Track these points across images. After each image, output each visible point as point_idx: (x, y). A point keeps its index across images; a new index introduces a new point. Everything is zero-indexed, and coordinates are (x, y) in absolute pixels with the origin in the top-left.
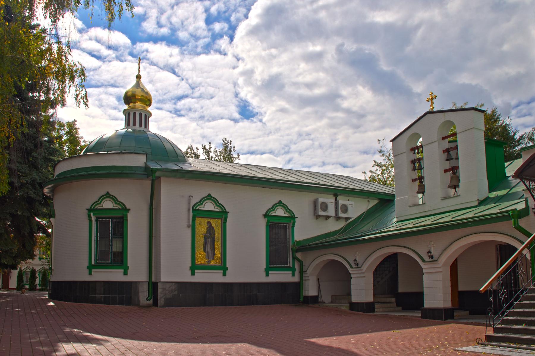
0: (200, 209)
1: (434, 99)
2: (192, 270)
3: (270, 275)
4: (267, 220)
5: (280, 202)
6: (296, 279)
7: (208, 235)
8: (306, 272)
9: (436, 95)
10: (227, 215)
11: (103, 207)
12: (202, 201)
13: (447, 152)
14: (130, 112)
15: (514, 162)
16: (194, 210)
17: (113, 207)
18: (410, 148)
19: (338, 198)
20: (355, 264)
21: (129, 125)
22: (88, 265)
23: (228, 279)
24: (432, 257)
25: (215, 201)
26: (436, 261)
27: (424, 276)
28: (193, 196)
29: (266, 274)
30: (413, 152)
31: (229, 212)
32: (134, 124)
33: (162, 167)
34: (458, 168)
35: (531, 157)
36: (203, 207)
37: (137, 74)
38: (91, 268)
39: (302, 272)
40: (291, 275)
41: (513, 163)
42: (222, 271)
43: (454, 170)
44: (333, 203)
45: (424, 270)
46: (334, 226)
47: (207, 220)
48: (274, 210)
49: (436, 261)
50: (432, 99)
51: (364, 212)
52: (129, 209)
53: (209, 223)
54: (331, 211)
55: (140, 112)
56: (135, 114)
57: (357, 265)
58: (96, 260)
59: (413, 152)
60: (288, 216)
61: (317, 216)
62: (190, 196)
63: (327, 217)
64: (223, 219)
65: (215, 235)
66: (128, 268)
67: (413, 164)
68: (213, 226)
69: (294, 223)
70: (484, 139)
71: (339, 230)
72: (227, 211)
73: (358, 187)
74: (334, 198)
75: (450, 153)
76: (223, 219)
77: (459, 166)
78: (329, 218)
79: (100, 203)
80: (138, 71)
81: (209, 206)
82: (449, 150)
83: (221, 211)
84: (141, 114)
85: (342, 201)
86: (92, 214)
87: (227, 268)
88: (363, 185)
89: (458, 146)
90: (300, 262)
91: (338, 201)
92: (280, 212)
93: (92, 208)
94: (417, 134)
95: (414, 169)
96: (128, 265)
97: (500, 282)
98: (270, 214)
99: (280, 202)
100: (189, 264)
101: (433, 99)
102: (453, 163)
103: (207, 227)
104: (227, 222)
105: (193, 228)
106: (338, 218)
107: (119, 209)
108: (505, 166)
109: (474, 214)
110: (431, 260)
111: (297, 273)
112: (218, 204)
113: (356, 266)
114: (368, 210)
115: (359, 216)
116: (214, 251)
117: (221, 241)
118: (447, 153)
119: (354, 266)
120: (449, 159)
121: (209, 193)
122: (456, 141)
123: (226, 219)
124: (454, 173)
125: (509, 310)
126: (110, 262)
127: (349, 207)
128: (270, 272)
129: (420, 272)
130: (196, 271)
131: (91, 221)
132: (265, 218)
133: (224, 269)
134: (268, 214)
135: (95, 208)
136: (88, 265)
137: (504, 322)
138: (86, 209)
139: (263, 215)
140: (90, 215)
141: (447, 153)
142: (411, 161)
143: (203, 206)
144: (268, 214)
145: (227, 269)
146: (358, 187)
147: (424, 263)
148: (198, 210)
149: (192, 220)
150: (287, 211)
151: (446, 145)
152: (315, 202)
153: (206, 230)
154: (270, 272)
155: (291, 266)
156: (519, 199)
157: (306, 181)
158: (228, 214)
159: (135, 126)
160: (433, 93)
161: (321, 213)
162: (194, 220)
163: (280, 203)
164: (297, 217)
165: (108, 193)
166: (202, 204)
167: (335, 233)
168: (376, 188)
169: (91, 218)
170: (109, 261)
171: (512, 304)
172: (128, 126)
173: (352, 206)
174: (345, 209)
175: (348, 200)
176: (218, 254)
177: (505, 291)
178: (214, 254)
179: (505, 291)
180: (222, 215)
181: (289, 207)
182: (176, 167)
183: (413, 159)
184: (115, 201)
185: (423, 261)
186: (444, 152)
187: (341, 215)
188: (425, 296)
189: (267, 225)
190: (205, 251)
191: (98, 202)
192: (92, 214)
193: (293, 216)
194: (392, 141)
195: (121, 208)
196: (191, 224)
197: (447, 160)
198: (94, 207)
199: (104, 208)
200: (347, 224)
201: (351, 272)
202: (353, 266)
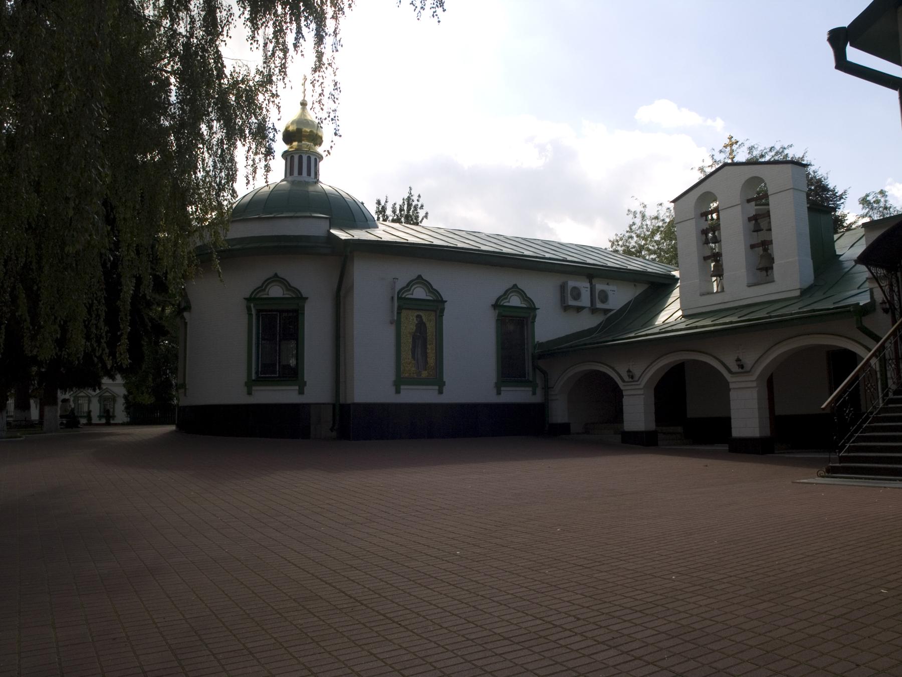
0: (407, 297)
1: (734, 145)
2: (248, 387)
3: (401, 390)
4: (499, 313)
5: (420, 277)
6: (537, 399)
7: (418, 334)
8: (553, 388)
9: (738, 140)
10: (444, 305)
11: (268, 295)
12: (409, 285)
13: (754, 220)
14: (294, 155)
15: (845, 235)
16: (399, 298)
17: (284, 294)
18: (700, 213)
19: (593, 281)
20: (629, 376)
21: (291, 173)
22: (246, 381)
23: (446, 398)
24: (742, 367)
25: (427, 285)
26: (749, 372)
27: (731, 393)
28: (398, 279)
29: (396, 389)
30: (704, 217)
31: (446, 301)
32: (300, 173)
33: (353, 236)
34: (771, 242)
35: (883, 235)
36: (410, 294)
37: (302, 99)
38: (250, 384)
39: (547, 389)
40: (531, 393)
41: (843, 236)
42: (437, 387)
43: (766, 245)
44: (587, 288)
45: (730, 384)
46: (587, 322)
47: (417, 313)
48: (507, 298)
49: (749, 372)
50: (732, 145)
51: (631, 301)
52: (307, 298)
53: (419, 317)
54: (585, 301)
55: (308, 155)
56: (300, 158)
57: (632, 377)
58: (257, 373)
59: (704, 217)
60: (431, 299)
61: (565, 307)
62: (394, 279)
63: (579, 309)
64: (438, 311)
65: (428, 335)
66: (305, 384)
67: (704, 235)
68: (424, 320)
69: (535, 317)
70: (806, 203)
71: (595, 327)
72: (536, 307)
73: (573, 257)
74: (588, 281)
75: (759, 221)
76: (438, 311)
77: (772, 241)
78: (582, 310)
79: (264, 290)
80: (303, 95)
81: (419, 293)
82: (758, 218)
83: (435, 299)
84: (309, 158)
85: (600, 286)
86: (252, 305)
87: (306, 382)
88: (611, 257)
89: (771, 212)
90: (544, 373)
91: (595, 285)
92: (515, 301)
93: (253, 296)
94: (714, 196)
95: (707, 242)
96: (305, 380)
97: (845, 398)
98: (501, 304)
99: (420, 277)
100: (392, 377)
101: (733, 145)
102: (762, 236)
103: (417, 322)
104: (443, 315)
105: (398, 324)
106: (594, 310)
107: (292, 298)
108: (835, 239)
109: (799, 309)
110: (740, 370)
111: (539, 391)
112: (431, 290)
113: (631, 380)
114: (636, 298)
115: (625, 305)
116: (426, 357)
117: (436, 343)
118: (754, 222)
119: (626, 378)
120: (757, 230)
121: (420, 274)
122: (768, 204)
123: (442, 310)
124: (766, 250)
125: (857, 435)
126: (260, 375)
127: (610, 294)
128: (502, 389)
129: (724, 388)
130: (402, 387)
131: (250, 315)
132: (494, 309)
133: (439, 382)
134: (499, 304)
135: (258, 296)
136: (246, 381)
137: (850, 450)
138: (244, 298)
139: (492, 305)
140: (250, 307)
141: (754, 222)
142: (702, 231)
143: (410, 292)
144: (499, 304)
145: (444, 384)
146: (573, 257)
147: (730, 375)
148: (405, 299)
149: (397, 313)
150: (430, 292)
151: (752, 209)
152: (563, 288)
153: (415, 328)
154: (502, 389)
155: (531, 379)
156: (859, 288)
157: (547, 255)
158: (446, 304)
159: (293, 175)
160: (732, 137)
161: (572, 302)
162: (399, 313)
163: (515, 289)
164: (539, 309)
165: (276, 275)
166: (410, 290)
167: (590, 332)
168: (511, 244)
169: (252, 311)
170: (276, 374)
171: (860, 427)
172: (290, 175)
173: (613, 292)
174: (604, 297)
175: (608, 284)
176: (431, 361)
177: (852, 409)
178: (426, 362)
179: (852, 409)
180: (437, 305)
181: (527, 293)
182: (829, 305)
183: (705, 228)
184: (429, 289)
185: (730, 371)
186: (750, 219)
187: (599, 305)
188: (732, 421)
189: (497, 320)
190: (413, 357)
191: (262, 288)
192: (252, 305)
193: (440, 299)
194: (674, 201)
195: (294, 296)
196: (396, 318)
197: (754, 231)
198: (256, 295)
199: (269, 297)
200: (607, 319)
201: (622, 388)
202: (625, 379)
